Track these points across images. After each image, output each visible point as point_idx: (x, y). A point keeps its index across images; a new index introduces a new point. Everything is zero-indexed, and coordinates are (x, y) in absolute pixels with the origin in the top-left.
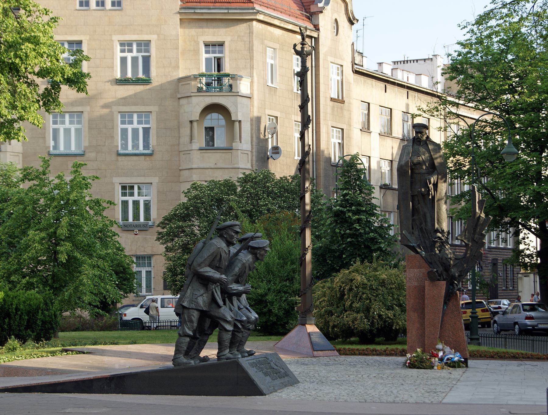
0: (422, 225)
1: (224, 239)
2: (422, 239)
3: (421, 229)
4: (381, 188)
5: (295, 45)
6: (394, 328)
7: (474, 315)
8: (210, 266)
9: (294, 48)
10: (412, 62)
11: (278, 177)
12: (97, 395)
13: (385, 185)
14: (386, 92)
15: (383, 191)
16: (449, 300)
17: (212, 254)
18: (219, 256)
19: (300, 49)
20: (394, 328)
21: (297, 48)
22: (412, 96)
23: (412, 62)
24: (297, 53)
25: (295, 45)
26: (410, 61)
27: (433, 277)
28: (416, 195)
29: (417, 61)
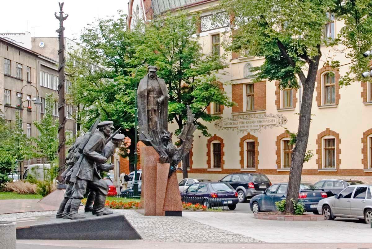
0: (154, 129)
1: (103, 133)
2: (154, 137)
3: (153, 131)
4: (5, 106)
5: (56, 13)
6: (133, 191)
7: (136, 184)
8: (95, 151)
9: (55, 15)
10: (12, 34)
11: (362, 88)
12: (119, 240)
13: (7, 104)
14: (8, 50)
15: (5, 108)
16: (171, 175)
17: (98, 143)
18: (102, 143)
19: (59, 16)
20: (133, 191)
21: (57, 15)
22: (22, 54)
23: (12, 34)
24: (57, 18)
25: (56, 13)
26: (9, 34)
27: (162, 161)
28: (151, 110)
29: (15, 34)
